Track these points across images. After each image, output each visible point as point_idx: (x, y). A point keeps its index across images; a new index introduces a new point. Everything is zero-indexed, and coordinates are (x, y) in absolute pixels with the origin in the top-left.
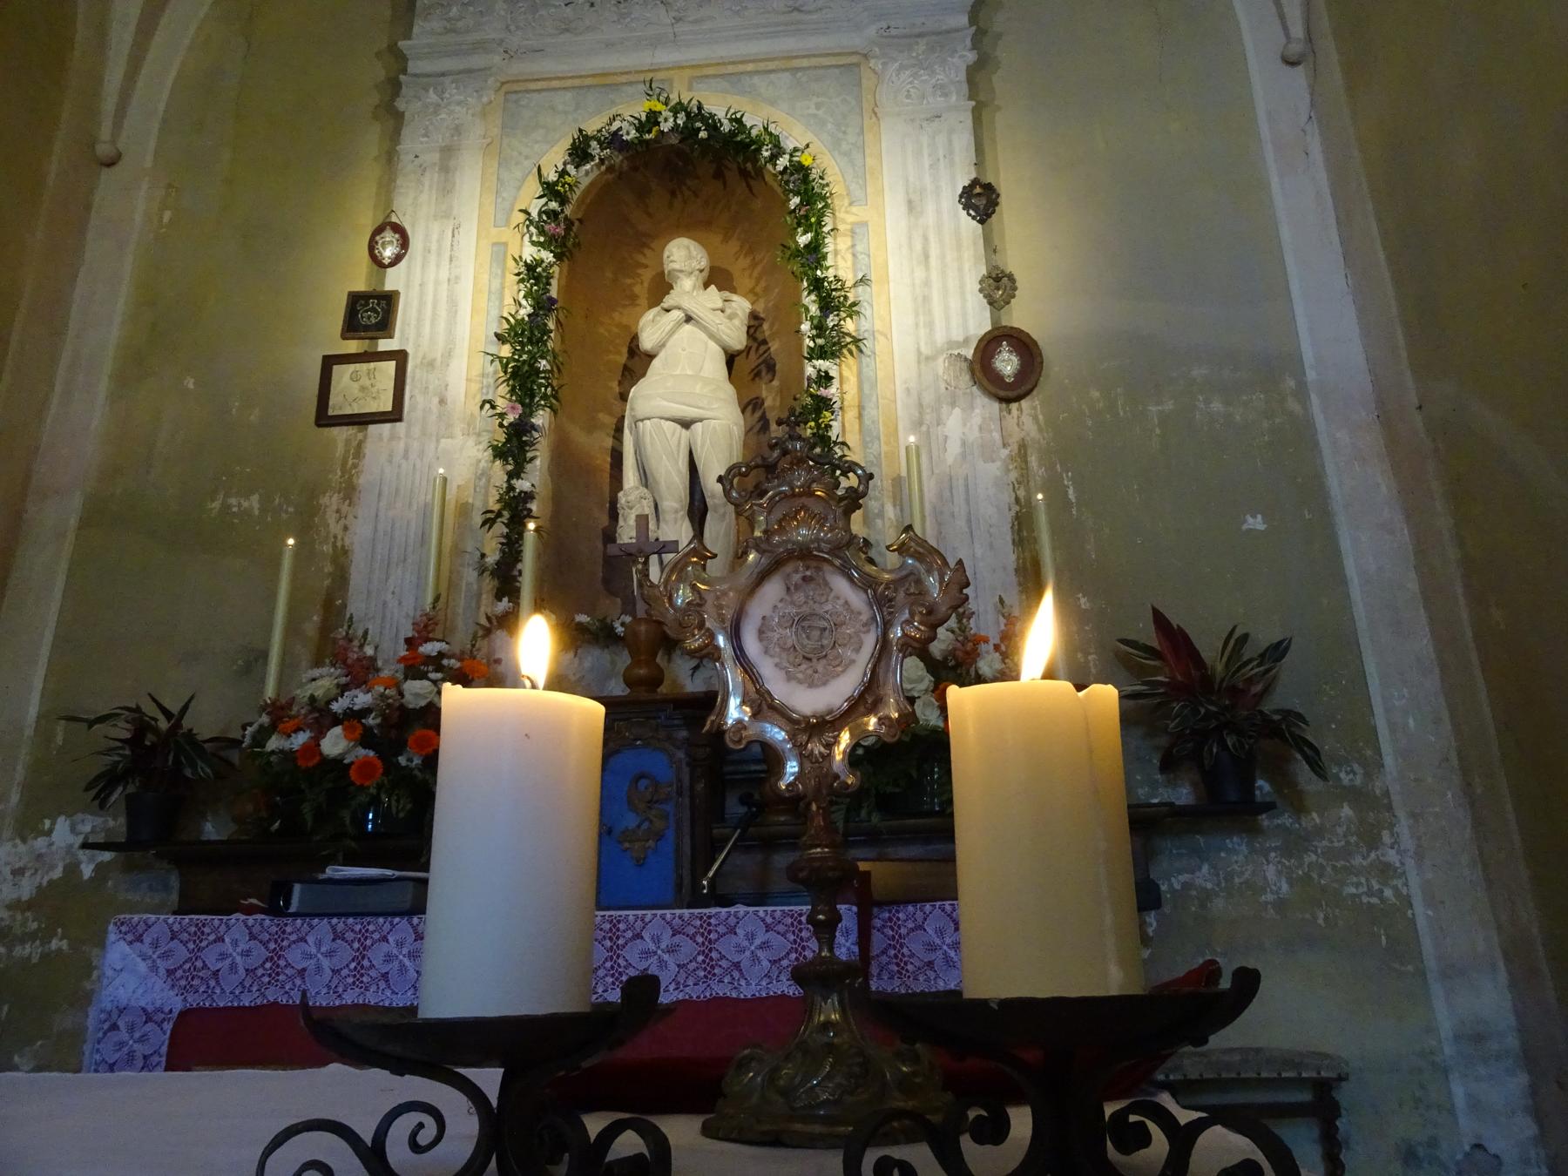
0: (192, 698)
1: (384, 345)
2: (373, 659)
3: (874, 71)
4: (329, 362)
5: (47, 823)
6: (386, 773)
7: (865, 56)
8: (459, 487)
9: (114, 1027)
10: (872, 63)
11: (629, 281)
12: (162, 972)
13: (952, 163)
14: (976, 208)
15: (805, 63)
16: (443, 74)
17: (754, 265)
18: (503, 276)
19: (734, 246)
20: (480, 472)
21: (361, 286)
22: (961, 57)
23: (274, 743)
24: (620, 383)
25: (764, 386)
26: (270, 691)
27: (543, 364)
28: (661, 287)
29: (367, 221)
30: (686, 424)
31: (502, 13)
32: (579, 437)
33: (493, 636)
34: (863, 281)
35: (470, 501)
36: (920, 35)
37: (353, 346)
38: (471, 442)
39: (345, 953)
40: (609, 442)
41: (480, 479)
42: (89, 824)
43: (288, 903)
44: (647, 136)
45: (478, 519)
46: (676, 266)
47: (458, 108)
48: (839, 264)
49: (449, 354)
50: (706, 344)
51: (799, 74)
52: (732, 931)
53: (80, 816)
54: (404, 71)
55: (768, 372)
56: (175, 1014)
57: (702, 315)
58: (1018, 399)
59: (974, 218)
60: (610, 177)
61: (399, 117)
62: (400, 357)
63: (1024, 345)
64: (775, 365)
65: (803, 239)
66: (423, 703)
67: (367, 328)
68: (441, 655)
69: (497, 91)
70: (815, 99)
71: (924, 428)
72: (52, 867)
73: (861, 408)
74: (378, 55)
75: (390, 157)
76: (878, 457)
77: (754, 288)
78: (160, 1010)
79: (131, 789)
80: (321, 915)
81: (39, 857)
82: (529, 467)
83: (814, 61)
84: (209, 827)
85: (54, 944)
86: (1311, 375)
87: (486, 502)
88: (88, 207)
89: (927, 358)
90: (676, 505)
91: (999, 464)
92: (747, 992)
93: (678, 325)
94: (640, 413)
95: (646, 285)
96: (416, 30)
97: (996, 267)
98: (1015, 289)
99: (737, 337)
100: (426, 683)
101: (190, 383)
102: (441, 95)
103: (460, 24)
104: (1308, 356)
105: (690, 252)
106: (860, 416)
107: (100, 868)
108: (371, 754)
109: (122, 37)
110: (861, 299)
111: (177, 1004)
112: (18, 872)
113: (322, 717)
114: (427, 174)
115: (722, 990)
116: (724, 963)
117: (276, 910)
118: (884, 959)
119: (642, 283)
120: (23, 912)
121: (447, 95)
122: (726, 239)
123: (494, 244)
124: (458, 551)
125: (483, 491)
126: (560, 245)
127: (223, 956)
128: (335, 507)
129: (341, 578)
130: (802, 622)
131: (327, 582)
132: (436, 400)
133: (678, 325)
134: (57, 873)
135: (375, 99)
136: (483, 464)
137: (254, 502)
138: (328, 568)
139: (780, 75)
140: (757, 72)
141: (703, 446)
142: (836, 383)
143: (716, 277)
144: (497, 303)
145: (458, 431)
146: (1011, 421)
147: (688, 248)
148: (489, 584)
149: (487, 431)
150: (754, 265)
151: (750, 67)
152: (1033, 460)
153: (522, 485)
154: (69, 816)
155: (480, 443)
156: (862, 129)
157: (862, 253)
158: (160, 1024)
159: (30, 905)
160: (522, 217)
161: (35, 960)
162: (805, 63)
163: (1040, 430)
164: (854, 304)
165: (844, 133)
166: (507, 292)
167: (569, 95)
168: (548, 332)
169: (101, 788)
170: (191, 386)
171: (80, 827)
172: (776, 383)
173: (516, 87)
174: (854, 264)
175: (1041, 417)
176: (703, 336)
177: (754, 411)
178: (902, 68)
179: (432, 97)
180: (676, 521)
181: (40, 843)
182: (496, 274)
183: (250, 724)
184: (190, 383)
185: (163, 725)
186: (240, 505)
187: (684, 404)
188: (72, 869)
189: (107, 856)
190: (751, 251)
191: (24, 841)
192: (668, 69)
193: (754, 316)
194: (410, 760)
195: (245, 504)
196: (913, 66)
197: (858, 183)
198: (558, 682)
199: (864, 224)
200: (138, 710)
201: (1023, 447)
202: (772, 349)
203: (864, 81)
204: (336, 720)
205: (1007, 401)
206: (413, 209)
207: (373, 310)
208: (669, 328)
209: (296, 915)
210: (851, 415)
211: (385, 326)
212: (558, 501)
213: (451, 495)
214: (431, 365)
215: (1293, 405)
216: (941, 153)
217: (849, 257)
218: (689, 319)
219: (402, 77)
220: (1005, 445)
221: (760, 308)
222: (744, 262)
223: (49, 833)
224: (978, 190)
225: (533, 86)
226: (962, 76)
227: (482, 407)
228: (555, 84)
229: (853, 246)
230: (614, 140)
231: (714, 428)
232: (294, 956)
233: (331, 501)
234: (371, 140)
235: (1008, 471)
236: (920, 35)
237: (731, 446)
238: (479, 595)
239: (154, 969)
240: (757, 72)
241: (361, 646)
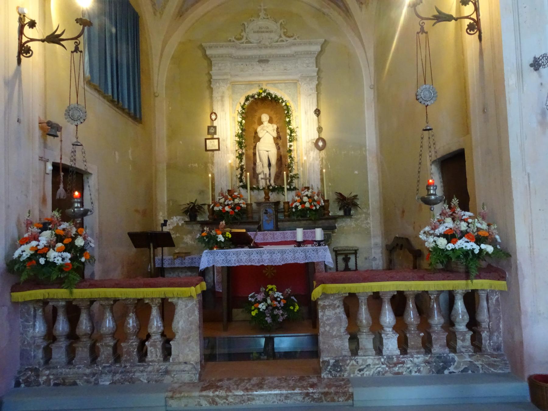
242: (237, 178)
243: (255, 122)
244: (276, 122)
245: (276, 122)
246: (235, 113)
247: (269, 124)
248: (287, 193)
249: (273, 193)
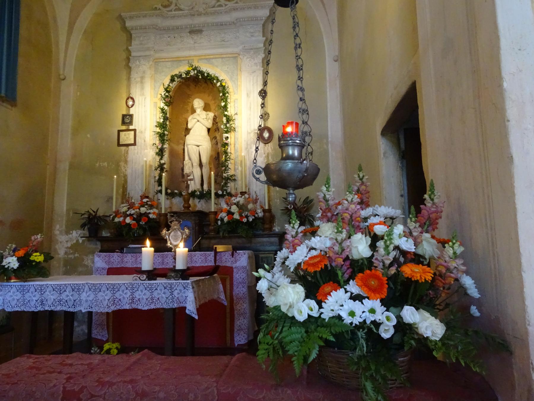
0: (98, 209)
1: (131, 127)
2: (134, 202)
3: (241, 58)
4: (119, 131)
5: (71, 232)
6: (138, 225)
7: (239, 55)
8: (149, 161)
9: (98, 270)
10: (240, 56)
11: (186, 107)
12: (104, 262)
13: (257, 84)
14: (262, 96)
15: (225, 56)
16: (140, 56)
17: (215, 103)
19: (211, 98)
21: (125, 113)
22: (261, 55)
23: (117, 220)
24: (185, 132)
26: (114, 209)
27: (166, 132)
28: (194, 111)
29: (125, 97)
30: (198, 146)
31: (153, 39)
32: (175, 147)
34: (236, 114)
36: (252, 49)
37: (124, 128)
38: (151, 150)
39: (134, 259)
40: (182, 147)
42: (80, 232)
43: (123, 251)
44: (188, 76)
45: (154, 169)
47: (144, 66)
48: (230, 111)
49: (145, 130)
51: (223, 59)
52: (195, 256)
53: (78, 230)
54: (131, 56)
56: (107, 269)
58: (268, 143)
59: (261, 98)
60: (181, 83)
61: (130, 68)
62: (135, 130)
63: (270, 131)
65: (223, 104)
66: (144, 212)
67: (127, 123)
68: (147, 201)
69: (153, 61)
70: (227, 66)
71: (248, 150)
72: (73, 240)
73: (235, 144)
74: (124, 51)
75: (129, 79)
76: (238, 156)
78: (104, 268)
79: (89, 226)
80: (129, 253)
81: (71, 239)
82: (164, 157)
83: (228, 56)
84: (103, 233)
85: (76, 255)
86: (330, 139)
87: (155, 165)
88: (60, 91)
89: (249, 133)
90: (196, 164)
91: (263, 158)
92: (197, 265)
94: (188, 144)
95: (190, 107)
96: (133, 43)
97: (266, 111)
98: (269, 117)
99: (209, 124)
100: (144, 208)
101: (89, 136)
102: (139, 62)
103: (143, 42)
104: (329, 136)
106: (234, 146)
107: (83, 241)
108: (135, 222)
109: (62, 46)
111: (107, 267)
112: (67, 241)
113: (125, 215)
114: (138, 84)
115: (194, 265)
116: (194, 261)
117: (122, 252)
118: (219, 260)
120: (69, 249)
121: (141, 62)
122: (209, 96)
123: (155, 102)
124: (150, 175)
126: (168, 104)
127: (114, 260)
128: (123, 165)
129: (126, 181)
130: (175, 236)
131: (123, 182)
132: (143, 141)
134: (75, 241)
135: (124, 63)
137: (106, 164)
138: (123, 179)
139: (219, 59)
140: (213, 58)
142: (229, 138)
143: (206, 108)
145: (148, 147)
146: (266, 148)
147: (199, 102)
148: (156, 184)
150: (215, 103)
151: (212, 57)
152: (270, 158)
153: (162, 162)
154: (75, 230)
156: (237, 74)
158: (105, 270)
159: (70, 248)
160: (160, 96)
161: (73, 258)
162: (225, 56)
163: (272, 151)
164: (234, 120)
165: (233, 75)
167: (170, 63)
168: (167, 125)
169: (83, 226)
170: (89, 136)
171: (78, 233)
172: (219, 134)
173: (157, 61)
175: (272, 147)
177: (215, 139)
178: (247, 58)
179: (138, 63)
180: (196, 168)
181: (70, 236)
183: (112, 215)
184: (89, 136)
185: (94, 214)
186: (103, 165)
188: (78, 241)
189: (84, 239)
190: (214, 99)
191: (67, 235)
192: (193, 57)
193: (215, 116)
194: (142, 223)
195: (104, 164)
196: (249, 58)
198: (151, 247)
199: (237, 99)
200: (88, 212)
201: (268, 154)
202: (219, 125)
203: (238, 62)
204: (128, 216)
205: (266, 144)
206: (135, 93)
207: (128, 119)
209: (125, 253)
210: (232, 146)
211: (131, 123)
212: (171, 163)
213: (148, 163)
214: (142, 132)
215: (325, 146)
216: (255, 82)
217: (234, 108)
218: (198, 121)
219: (130, 57)
220: (264, 154)
221: (216, 114)
222: (213, 102)
223: (72, 234)
224: (262, 92)
225: (161, 60)
226: (261, 61)
227: (153, 145)
228: (167, 60)
229: (234, 105)
230: (180, 76)
232: (125, 260)
233: (122, 164)
234: (124, 75)
235: (265, 160)
236: (252, 49)
237: (207, 152)
238: (155, 186)
239: (103, 261)
240: (213, 58)
241: (131, 200)
243: (188, 110)
244: (215, 109)
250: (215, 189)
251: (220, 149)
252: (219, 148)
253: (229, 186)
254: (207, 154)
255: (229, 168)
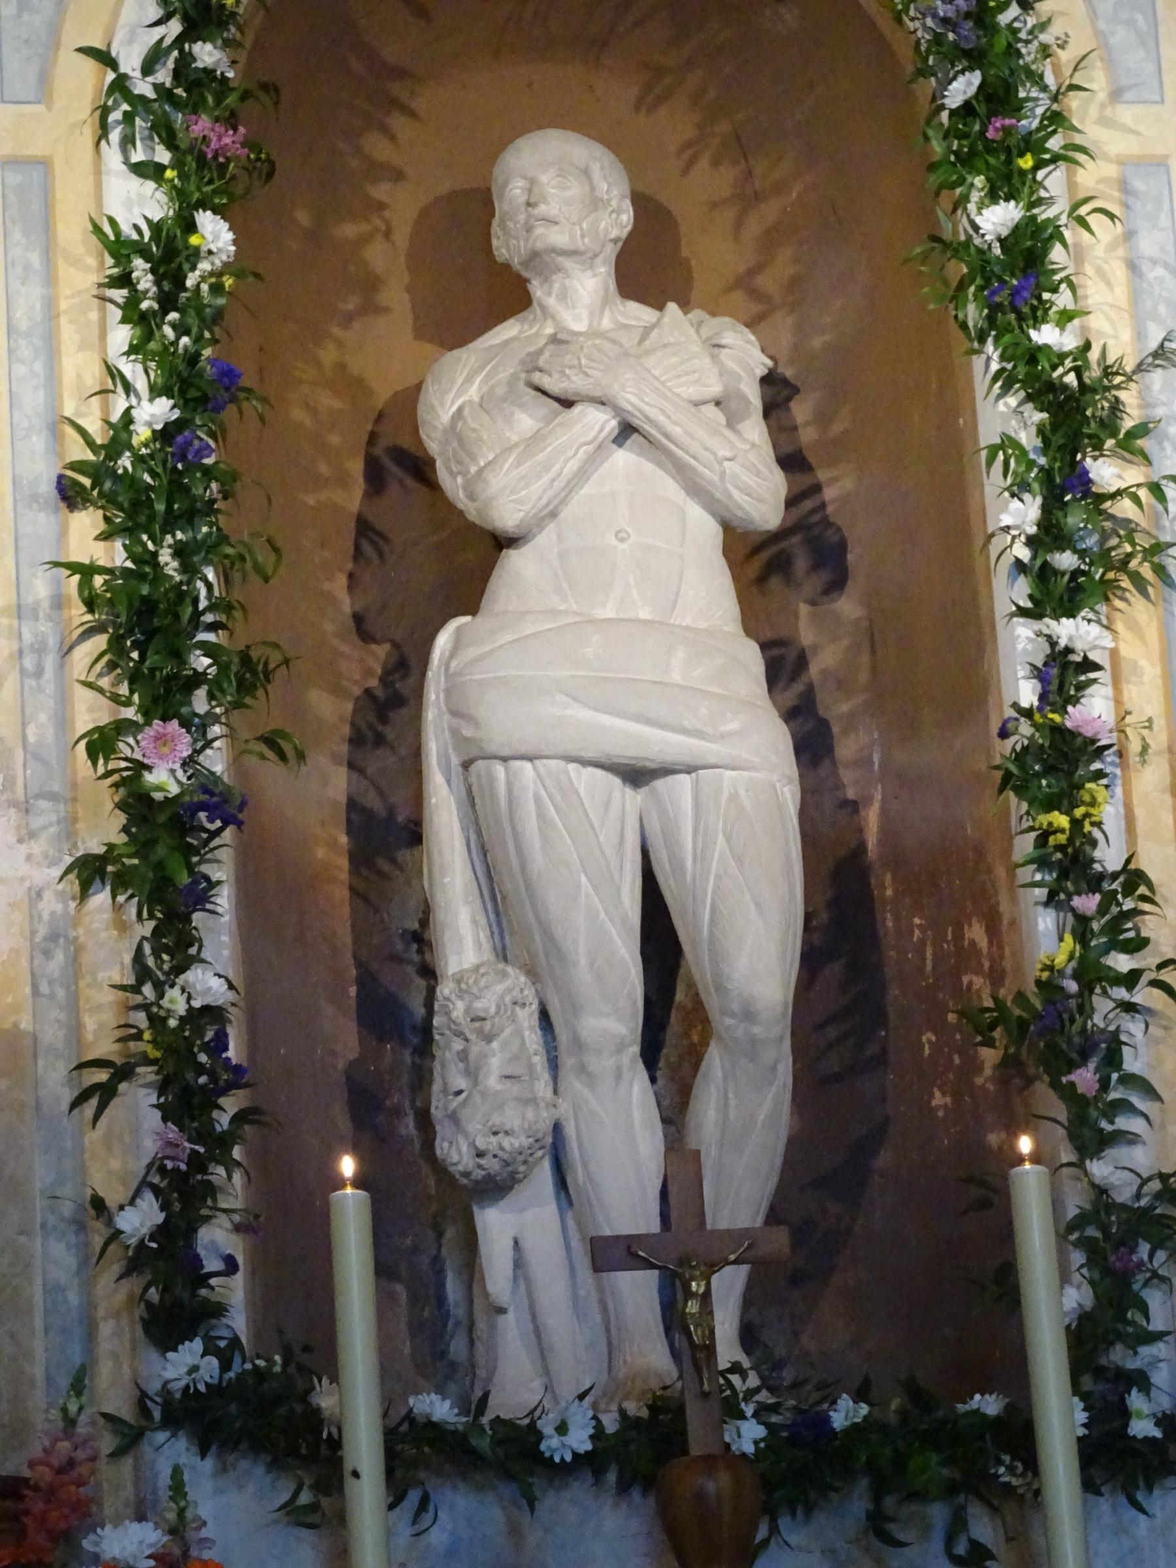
18: (50, 279)
20: (42, 931)
25: (804, 609)
33: (146, 1448)
35: (26, 1023)
41: (47, 954)
46: (558, 237)
50: (682, 511)
55: (815, 567)
57: (676, 431)
64: (842, 547)
77: (753, 272)
93: (598, 454)
95: (402, 236)
105: (593, 188)
110: (1160, 412)
119: (388, 234)
125: (61, 993)
133: (598, 454)
136: (50, 905)
141: (701, 857)
144: (38, 367)
149: (53, 797)
155: (32, 835)
157: (1154, 262)
164: (1142, 430)
166: (68, 334)
174: (1135, 296)
176: (670, 488)
180: (618, 1077)
182: (27, 268)
187: (648, 722)
197: (1130, 23)
202: (829, 493)
208: (573, 465)
217: (1119, 272)
218: (627, 431)
231: (734, 797)
242: (91, 1261)
243: (370, 285)
244: (745, 283)
245: (745, 283)
246: (44, 90)
247: (639, 313)
248: (1087, 1517)
249: (1152, 1380)
250: (387, 1371)
251: (872, 817)
252: (853, 807)
253: (1158, 1323)
254: (428, 851)
255: (1130, 1080)
